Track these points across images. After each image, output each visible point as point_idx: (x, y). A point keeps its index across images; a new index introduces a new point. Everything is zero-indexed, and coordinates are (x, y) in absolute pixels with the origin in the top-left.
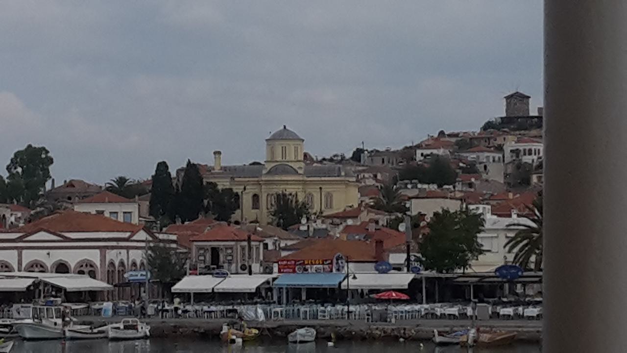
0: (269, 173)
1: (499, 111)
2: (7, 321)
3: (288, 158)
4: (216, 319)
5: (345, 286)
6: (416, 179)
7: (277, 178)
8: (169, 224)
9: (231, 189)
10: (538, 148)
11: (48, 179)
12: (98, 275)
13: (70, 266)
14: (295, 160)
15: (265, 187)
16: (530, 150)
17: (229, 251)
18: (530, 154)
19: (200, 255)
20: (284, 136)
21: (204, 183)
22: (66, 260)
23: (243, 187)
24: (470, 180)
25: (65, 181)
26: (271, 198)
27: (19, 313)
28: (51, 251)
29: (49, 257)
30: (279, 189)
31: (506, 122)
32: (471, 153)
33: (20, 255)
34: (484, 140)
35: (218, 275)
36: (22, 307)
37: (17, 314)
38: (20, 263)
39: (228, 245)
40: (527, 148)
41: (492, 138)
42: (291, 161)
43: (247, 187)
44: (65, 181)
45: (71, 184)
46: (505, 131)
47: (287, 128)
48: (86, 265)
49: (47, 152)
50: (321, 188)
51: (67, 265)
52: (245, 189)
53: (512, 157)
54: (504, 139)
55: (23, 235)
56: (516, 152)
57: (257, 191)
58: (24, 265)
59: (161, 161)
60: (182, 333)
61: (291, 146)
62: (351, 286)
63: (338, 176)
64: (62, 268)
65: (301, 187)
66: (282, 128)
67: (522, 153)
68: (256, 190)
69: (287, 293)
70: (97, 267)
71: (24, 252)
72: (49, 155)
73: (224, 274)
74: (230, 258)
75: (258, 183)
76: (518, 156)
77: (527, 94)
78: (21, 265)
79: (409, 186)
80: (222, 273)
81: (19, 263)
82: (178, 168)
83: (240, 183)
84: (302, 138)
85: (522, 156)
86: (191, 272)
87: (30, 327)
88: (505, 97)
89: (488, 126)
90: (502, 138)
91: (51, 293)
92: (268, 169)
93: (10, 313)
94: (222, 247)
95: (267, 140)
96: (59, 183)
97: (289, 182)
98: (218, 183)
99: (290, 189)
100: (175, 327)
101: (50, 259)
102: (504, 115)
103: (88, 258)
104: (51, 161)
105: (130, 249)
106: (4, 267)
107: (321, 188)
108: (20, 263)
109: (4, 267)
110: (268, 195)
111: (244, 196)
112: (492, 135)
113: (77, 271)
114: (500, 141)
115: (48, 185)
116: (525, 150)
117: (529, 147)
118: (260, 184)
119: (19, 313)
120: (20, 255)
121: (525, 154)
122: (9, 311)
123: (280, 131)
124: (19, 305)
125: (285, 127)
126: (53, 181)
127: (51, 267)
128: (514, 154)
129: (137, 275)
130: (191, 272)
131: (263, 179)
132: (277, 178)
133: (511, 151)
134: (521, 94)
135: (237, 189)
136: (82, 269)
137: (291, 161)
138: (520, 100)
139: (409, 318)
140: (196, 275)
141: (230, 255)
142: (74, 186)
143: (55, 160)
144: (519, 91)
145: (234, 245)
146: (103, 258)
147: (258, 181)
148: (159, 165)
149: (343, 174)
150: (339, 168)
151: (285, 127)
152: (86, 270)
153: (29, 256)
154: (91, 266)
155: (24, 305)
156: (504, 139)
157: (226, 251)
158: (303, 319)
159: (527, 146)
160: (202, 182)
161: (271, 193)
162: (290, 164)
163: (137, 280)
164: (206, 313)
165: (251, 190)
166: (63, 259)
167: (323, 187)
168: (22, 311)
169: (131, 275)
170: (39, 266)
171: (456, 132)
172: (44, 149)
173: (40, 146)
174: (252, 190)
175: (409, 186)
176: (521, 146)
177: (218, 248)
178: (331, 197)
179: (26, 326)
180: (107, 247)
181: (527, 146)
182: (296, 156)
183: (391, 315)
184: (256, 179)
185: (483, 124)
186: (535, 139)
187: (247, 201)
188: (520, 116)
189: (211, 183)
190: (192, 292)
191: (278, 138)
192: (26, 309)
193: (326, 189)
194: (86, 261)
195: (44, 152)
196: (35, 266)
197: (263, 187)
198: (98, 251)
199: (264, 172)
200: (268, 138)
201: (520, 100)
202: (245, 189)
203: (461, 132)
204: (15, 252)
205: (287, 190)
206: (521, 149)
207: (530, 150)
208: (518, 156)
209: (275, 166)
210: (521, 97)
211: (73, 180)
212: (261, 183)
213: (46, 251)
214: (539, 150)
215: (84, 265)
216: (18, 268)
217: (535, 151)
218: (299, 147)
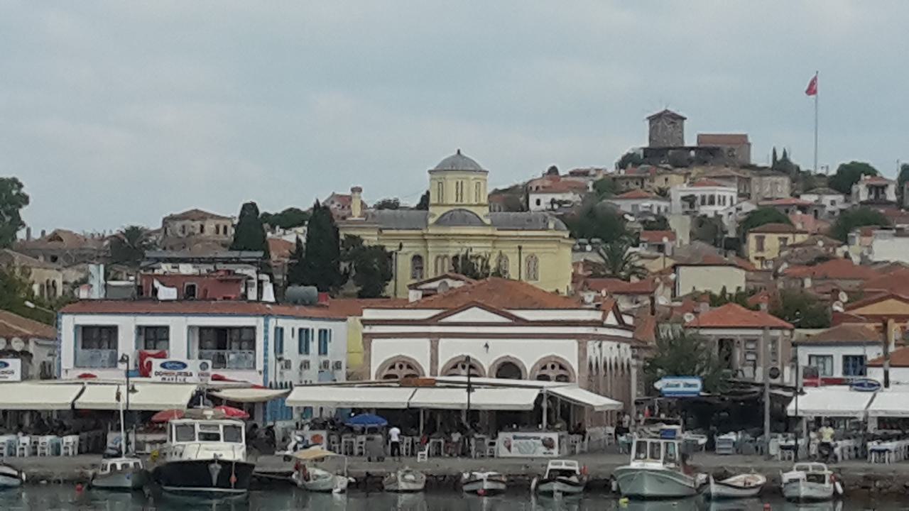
0: (438, 223)
1: (639, 141)
2: (561, 464)
3: (465, 202)
4: (21, 459)
5: (792, 411)
6: (599, 237)
7: (453, 230)
8: (783, 302)
9: (383, 248)
10: (722, 194)
11: (20, 227)
12: (216, 385)
13: (523, 366)
14: (476, 203)
15: (434, 245)
16: (712, 197)
17: (751, 346)
18: (712, 202)
19: (749, 352)
20: (458, 165)
21: (342, 237)
22: (504, 354)
23: (398, 244)
24: (661, 240)
25: (43, 233)
26: (443, 262)
27: (509, 448)
28: (491, 342)
29: (487, 350)
30: (454, 249)
31: (653, 154)
32: (644, 200)
33: (434, 349)
34: (635, 181)
35: (861, 387)
36: (515, 438)
37: (506, 450)
38: (434, 360)
39: (726, 335)
40: (708, 194)
41: (646, 178)
42: (471, 205)
43: (404, 245)
44: (43, 233)
45: (56, 237)
46: (666, 169)
47: (462, 152)
48: (553, 367)
49: (21, 186)
50: (520, 248)
51: (520, 366)
52: (401, 247)
53: (683, 206)
54: (666, 180)
55: (440, 314)
56: (690, 200)
57: (419, 250)
58: (441, 365)
59: (248, 201)
60: (880, 489)
61: (470, 181)
62: (133, 405)
63: (543, 230)
64: (508, 369)
65: (489, 245)
66: (456, 153)
67: (699, 201)
68: (417, 250)
69: (424, 412)
70: (573, 370)
71: (442, 341)
72: (24, 190)
73: (873, 385)
74: (751, 357)
75: (424, 239)
76: (692, 206)
77: (681, 113)
78: (437, 363)
79: (589, 248)
80: (869, 384)
81: (432, 364)
82: (165, 216)
83: (392, 238)
84: (484, 168)
85: (699, 206)
86: (806, 381)
87: (653, 475)
88: (649, 118)
89: (626, 161)
90: (662, 178)
91: (659, 415)
92: (438, 215)
93: (495, 447)
94: (739, 338)
95: (430, 172)
96: (36, 235)
97: (500, 238)
98: (363, 237)
99: (478, 249)
100: (866, 478)
101: (487, 355)
102: (646, 144)
103: (556, 354)
104: (25, 200)
105: (374, 338)
106: (405, 367)
107: (520, 248)
108: (434, 360)
109: (405, 367)
110: (438, 257)
111: (400, 258)
112: (649, 174)
113: (536, 377)
114: (659, 183)
115: (21, 234)
116: (703, 197)
117: (711, 193)
118: (426, 240)
119: (509, 448)
120: (434, 349)
121: (703, 203)
122: (492, 444)
123: (453, 157)
124: (510, 435)
125: (459, 152)
126: (28, 231)
127: (490, 369)
128: (687, 204)
129: (677, 386)
130: (806, 381)
131: (431, 231)
132: (453, 230)
133: (683, 198)
134: (674, 114)
135: (390, 247)
136: (544, 372)
137: (471, 205)
138: (672, 123)
139: (73, 453)
140: (816, 386)
141: (754, 353)
142: (61, 240)
143: (31, 200)
144: (669, 109)
145: (761, 336)
146: (583, 351)
147: (423, 235)
148: (245, 207)
149: (551, 226)
150: (546, 217)
151: (459, 152)
152: (552, 374)
153: (450, 350)
154: (409, 367)
155: (518, 434)
156: (666, 180)
157: (745, 345)
158: (30, 455)
159: (706, 191)
160: (338, 235)
161: (442, 254)
162: (472, 209)
163: (678, 393)
164: (873, 454)
165: (411, 249)
166: (512, 355)
167: (523, 245)
168: (515, 446)
169: (668, 386)
170: (557, 367)
171: (583, 167)
172: (14, 181)
173: (10, 176)
174: (410, 249)
175: (589, 248)
176: (698, 192)
177: (732, 340)
178: (536, 260)
179: (650, 475)
180: (586, 336)
181: (706, 191)
182: (478, 195)
183: (478, 454)
184: (419, 232)
185: (619, 158)
186: (716, 181)
187: (403, 266)
188: (671, 145)
189: (354, 238)
190: (823, 416)
191: (450, 168)
192: (524, 441)
193: (528, 249)
194: (553, 359)
195: (16, 186)
196: (460, 366)
197: (429, 245)
198: (574, 343)
199: (431, 221)
200: (432, 168)
201: (672, 123)
202: (401, 247)
203: (592, 168)
204: (426, 342)
205: (473, 250)
206: (698, 194)
207: (712, 197)
208: (692, 206)
209: (449, 212)
210: (673, 118)
211: (59, 230)
212: (426, 237)
213: (484, 341)
214: (724, 197)
215: (549, 365)
216: (431, 369)
217: (719, 196)
218: (482, 184)
